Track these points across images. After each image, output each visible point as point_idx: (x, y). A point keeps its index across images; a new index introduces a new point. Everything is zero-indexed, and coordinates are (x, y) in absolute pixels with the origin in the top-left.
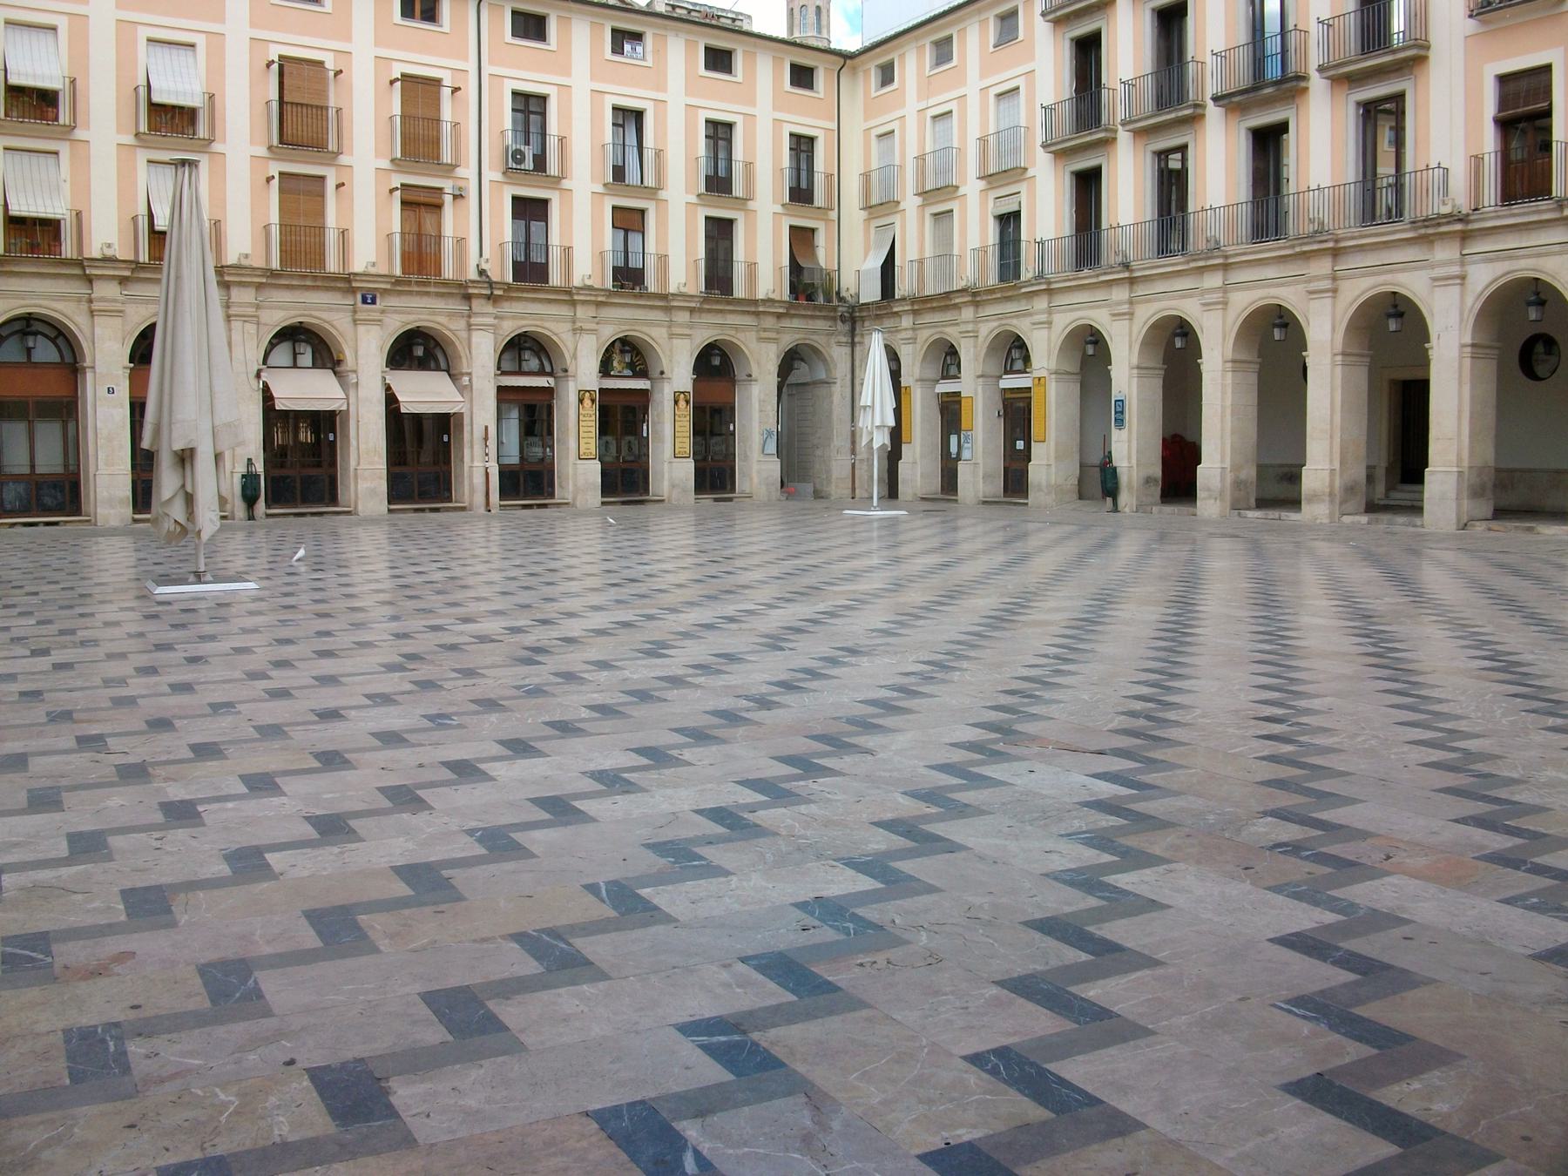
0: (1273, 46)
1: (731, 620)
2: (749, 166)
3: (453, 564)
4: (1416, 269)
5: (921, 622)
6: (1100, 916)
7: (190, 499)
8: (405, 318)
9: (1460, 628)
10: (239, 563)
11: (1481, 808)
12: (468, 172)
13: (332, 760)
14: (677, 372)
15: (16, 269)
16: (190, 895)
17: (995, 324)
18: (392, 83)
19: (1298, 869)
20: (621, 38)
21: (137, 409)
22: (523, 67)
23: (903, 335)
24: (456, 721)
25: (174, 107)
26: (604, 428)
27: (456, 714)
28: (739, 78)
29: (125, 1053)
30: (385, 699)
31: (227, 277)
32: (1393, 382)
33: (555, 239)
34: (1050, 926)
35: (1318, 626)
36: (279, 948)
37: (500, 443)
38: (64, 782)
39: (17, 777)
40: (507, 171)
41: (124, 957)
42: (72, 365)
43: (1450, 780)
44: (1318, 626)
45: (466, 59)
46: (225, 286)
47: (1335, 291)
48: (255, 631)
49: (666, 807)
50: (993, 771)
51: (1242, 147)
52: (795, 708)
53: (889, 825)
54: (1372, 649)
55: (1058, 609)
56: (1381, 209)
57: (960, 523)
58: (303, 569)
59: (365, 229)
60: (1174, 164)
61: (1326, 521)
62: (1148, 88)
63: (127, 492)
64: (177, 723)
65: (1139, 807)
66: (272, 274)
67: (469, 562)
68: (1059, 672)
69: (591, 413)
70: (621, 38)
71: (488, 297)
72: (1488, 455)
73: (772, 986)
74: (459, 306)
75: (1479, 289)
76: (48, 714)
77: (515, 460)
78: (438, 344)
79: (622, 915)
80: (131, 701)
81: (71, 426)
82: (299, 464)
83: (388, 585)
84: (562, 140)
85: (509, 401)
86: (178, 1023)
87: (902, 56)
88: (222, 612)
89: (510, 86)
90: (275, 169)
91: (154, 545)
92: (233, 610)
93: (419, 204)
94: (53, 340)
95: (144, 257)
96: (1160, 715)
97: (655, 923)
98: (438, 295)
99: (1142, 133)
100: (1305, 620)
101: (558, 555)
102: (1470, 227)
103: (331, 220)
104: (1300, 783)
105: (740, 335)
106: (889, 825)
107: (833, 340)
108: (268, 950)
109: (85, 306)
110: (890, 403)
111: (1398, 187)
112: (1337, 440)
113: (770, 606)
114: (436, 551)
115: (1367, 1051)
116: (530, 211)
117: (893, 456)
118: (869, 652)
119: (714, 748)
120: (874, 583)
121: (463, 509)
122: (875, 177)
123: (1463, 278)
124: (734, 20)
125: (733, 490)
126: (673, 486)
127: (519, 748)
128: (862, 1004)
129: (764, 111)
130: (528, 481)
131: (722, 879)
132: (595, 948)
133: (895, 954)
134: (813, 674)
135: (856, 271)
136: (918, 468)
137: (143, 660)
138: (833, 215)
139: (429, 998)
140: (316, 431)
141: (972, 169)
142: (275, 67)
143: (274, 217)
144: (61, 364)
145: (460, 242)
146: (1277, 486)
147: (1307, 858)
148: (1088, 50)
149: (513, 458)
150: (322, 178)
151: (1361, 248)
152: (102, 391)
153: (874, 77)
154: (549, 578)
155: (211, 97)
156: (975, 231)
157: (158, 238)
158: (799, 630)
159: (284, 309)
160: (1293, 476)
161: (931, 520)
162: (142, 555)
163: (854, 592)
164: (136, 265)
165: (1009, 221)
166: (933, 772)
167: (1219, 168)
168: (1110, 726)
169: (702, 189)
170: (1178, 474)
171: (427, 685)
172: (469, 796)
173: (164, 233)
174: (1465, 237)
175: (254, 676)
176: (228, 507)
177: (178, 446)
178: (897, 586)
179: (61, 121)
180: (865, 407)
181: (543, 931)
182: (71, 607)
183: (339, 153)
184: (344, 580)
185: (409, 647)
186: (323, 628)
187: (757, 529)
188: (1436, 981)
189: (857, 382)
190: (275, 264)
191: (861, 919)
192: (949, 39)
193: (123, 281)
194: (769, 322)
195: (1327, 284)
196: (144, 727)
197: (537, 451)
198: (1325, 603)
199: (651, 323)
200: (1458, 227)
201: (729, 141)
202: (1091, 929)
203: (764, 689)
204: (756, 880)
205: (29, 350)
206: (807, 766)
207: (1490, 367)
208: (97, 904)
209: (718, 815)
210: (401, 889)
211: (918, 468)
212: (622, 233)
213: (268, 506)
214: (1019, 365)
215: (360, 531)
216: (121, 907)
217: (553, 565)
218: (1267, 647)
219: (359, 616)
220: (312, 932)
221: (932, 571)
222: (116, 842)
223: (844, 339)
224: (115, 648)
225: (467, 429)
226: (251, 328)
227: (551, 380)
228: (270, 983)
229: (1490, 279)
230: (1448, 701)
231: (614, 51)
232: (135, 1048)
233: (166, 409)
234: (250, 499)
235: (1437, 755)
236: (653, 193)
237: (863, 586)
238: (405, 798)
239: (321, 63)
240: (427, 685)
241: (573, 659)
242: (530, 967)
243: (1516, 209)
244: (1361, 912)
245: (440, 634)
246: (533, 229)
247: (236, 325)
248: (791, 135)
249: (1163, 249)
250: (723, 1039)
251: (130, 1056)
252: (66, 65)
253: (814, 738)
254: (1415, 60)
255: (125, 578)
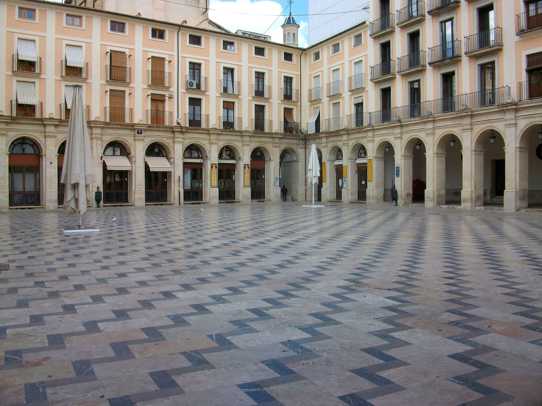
0: (449, 46)
1: (262, 243)
2: (270, 87)
3: (166, 223)
4: (499, 121)
5: (328, 244)
6: (387, 347)
7: (77, 200)
8: (152, 139)
9: (515, 245)
10: (94, 222)
11: (523, 309)
12: (174, 89)
13: (122, 291)
14: (245, 158)
15: (20, 122)
16: (71, 337)
17: (355, 141)
18: (148, 59)
19: (458, 331)
20: (226, 44)
21: (60, 169)
22: (194, 54)
23: (323, 145)
24: (166, 277)
25: (74, 67)
26: (220, 177)
27: (165, 275)
28: (266, 58)
29: (45, 393)
30: (141, 270)
31: (91, 125)
32: (492, 160)
33: (203, 112)
34: (370, 351)
35: (467, 246)
36: (101, 356)
37: (184, 182)
38: (29, 298)
39: (14, 296)
40: (187, 89)
41: (46, 359)
42: (38, 154)
43: (512, 299)
44: (467, 246)
45: (173, 51)
46: (90, 128)
47: (472, 129)
48: (98, 246)
49: (237, 308)
50: (352, 296)
51: (439, 80)
52: (283, 274)
53: (315, 315)
54: (485, 253)
55: (376, 239)
56: (487, 101)
57: (343, 209)
58: (115, 225)
59: (139, 108)
60: (416, 86)
61: (470, 209)
62: (406, 61)
63: (56, 197)
64: (70, 278)
65: (403, 309)
66: (107, 124)
67: (173, 222)
68: (375, 261)
69: (215, 172)
70: (226, 44)
71: (180, 132)
72: (526, 185)
73: (272, 371)
74: (170, 135)
75: (522, 128)
76: (25, 274)
77: (189, 188)
78: (163, 148)
79: (220, 346)
80: (54, 270)
81: (37, 175)
82: (115, 188)
83: (145, 230)
84: (206, 78)
85: (187, 167)
86: (63, 382)
87: (322, 50)
88: (88, 239)
89: (188, 60)
90: (108, 88)
91: (65, 216)
92: (91, 239)
93: (157, 100)
94: (32, 146)
95: (63, 118)
96: (411, 276)
97: (231, 349)
98: (163, 131)
99: (404, 76)
100: (462, 243)
101: (203, 220)
102: (518, 107)
103: (127, 105)
104: (459, 300)
105: (267, 145)
106: (315, 315)
107: (299, 147)
108: (97, 357)
109: (43, 134)
110: (318, 168)
111: (493, 93)
112: (473, 181)
113: (276, 238)
114: (161, 219)
115: (481, 396)
116: (195, 103)
117: (320, 186)
118: (309, 254)
119: (255, 288)
120: (313, 230)
121: (171, 204)
122: (313, 91)
123: (516, 124)
124: (265, 38)
125: (264, 198)
126: (243, 197)
127: (187, 287)
128: (304, 378)
129: (245, 62)
130: (194, 195)
131: (255, 334)
132: (209, 357)
133: (315, 360)
134: (290, 262)
135: (306, 121)
136: (328, 191)
137: (59, 256)
138: (299, 104)
139: (152, 374)
140: (121, 177)
141: (346, 88)
142: (109, 54)
143: (108, 105)
144: (35, 154)
145: (171, 113)
146: (452, 196)
147: (461, 327)
148: (386, 48)
149: (189, 187)
150: (124, 91)
151: (480, 115)
152: (48, 163)
153: (313, 57)
154: (200, 228)
155: (87, 64)
156: (347, 109)
157: (68, 111)
158: (285, 247)
159: (111, 135)
160: (458, 193)
161: (333, 209)
162: (60, 219)
163: (305, 233)
164: (60, 121)
165: (359, 106)
166: (331, 297)
167: (431, 87)
168: (393, 280)
169: (254, 95)
170: (418, 192)
171: (156, 265)
172: (169, 304)
173: (70, 110)
174: (516, 110)
175: (96, 261)
176: (91, 203)
177: (73, 182)
178: (321, 231)
179: (36, 72)
180: (310, 170)
181: (192, 351)
182: (35, 237)
183: (130, 83)
184: (129, 229)
185: (151, 252)
186: (121, 245)
187: (273, 212)
188: (506, 371)
189: (307, 161)
190: (108, 120)
191: (304, 348)
192: (338, 44)
193: (56, 126)
194: (277, 140)
195: (469, 127)
196: (58, 279)
197: (197, 185)
198: (469, 237)
199: (236, 141)
200: (514, 107)
201: (263, 79)
202: (384, 352)
203: (273, 267)
204: (268, 334)
205: (24, 149)
206: (287, 294)
207: (526, 155)
208: (38, 340)
209: (255, 311)
210: (144, 336)
211: (328, 191)
212: (226, 110)
213: (104, 203)
214: (363, 155)
215: (136, 212)
216: (47, 341)
217: (201, 224)
218: (448, 253)
219: (134, 241)
220: (112, 351)
221: (332, 226)
222: (46, 318)
223: (302, 146)
224: (50, 251)
225: (173, 177)
226: (99, 142)
227: (202, 160)
228: (97, 369)
229: (526, 124)
230: (512, 271)
231: (224, 49)
232: (49, 391)
233: (69, 170)
234: (98, 200)
235: (508, 291)
236: (237, 96)
237: (309, 231)
238: (147, 304)
239: (125, 53)
240: (156, 265)
241: (207, 257)
242: (187, 364)
243: (534, 101)
244: (480, 346)
245: (161, 247)
246: (196, 109)
247: (176, 144)
248: (284, 77)
249: (412, 115)
250: (254, 390)
251: (47, 393)
252: (38, 52)
253: (290, 284)
254: (498, 50)
255: (54, 227)
